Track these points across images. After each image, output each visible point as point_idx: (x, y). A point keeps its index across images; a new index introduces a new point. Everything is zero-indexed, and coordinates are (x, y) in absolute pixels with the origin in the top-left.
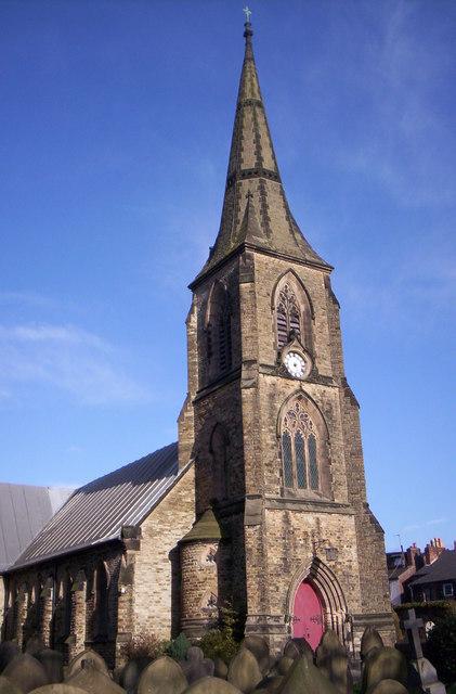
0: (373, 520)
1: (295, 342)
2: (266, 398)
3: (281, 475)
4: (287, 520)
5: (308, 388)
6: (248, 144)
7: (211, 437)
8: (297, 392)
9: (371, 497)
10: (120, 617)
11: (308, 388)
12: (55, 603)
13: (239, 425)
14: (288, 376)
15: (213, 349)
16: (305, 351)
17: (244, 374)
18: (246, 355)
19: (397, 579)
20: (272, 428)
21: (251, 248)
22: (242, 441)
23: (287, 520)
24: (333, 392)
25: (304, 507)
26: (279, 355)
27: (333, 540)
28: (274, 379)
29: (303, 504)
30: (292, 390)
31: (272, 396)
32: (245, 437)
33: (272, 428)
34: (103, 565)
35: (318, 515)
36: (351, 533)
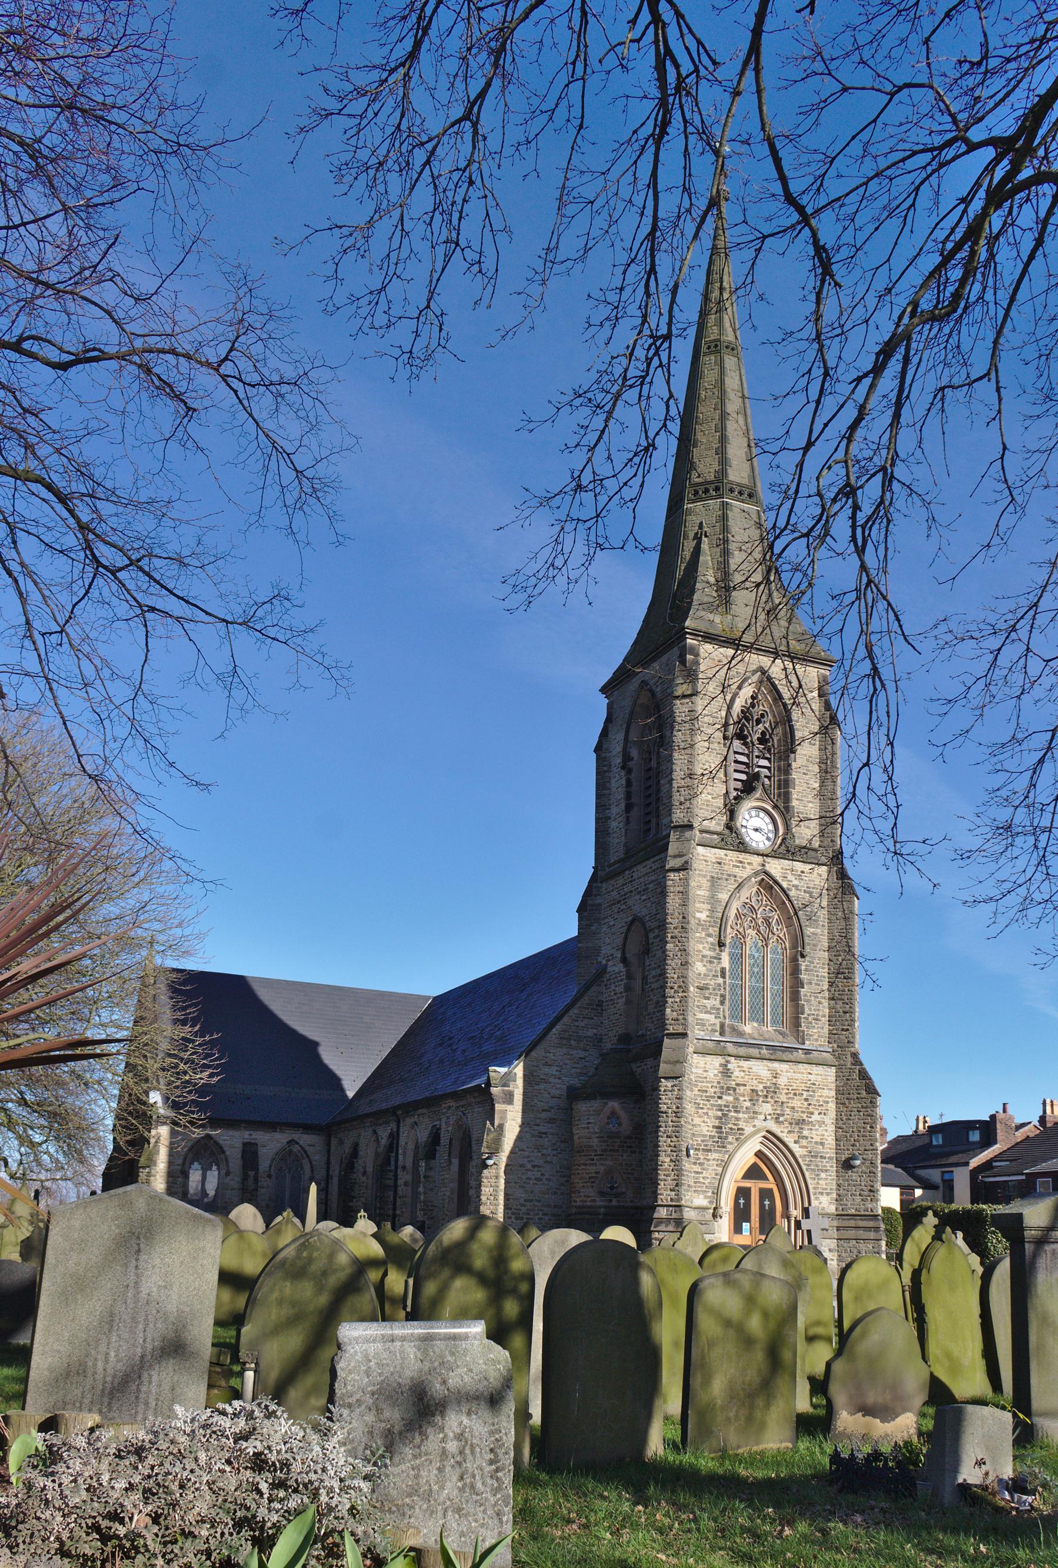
0: (864, 1075)
1: (759, 793)
2: (705, 883)
3: (722, 1003)
4: (726, 1072)
5: (776, 867)
6: (705, 436)
7: (626, 939)
8: (756, 874)
9: (861, 1044)
10: (483, 1198)
11: (776, 867)
12: (987, 192)
13: (663, 926)
14: (742, 847)
15: (634, 800)
16: (775, 807)
17: (672, 849)
18: (678, 816)
19: (967, 1164)
20: (711, 930)
21: (695, 634)
22: (664, 951)
23: (726, 1072)
24: (818, 876)
25: (754, 1052)
26: (732, 814)
27: (797, 1103)
28: (722, 852)
29: (750, 1050)
30: (748, 871)
31: (714, 881)
32: (669, 946)
33: (711, 930)
34: (307, 1191)
35: (776, 1065)
36: (828, 1093)
